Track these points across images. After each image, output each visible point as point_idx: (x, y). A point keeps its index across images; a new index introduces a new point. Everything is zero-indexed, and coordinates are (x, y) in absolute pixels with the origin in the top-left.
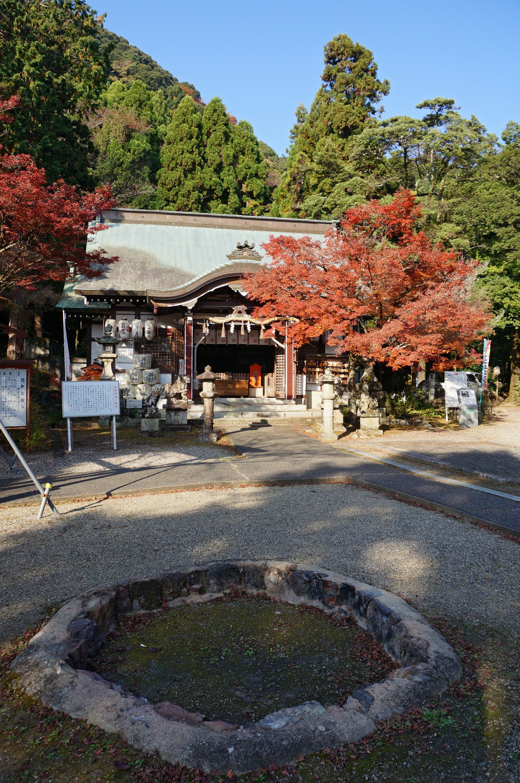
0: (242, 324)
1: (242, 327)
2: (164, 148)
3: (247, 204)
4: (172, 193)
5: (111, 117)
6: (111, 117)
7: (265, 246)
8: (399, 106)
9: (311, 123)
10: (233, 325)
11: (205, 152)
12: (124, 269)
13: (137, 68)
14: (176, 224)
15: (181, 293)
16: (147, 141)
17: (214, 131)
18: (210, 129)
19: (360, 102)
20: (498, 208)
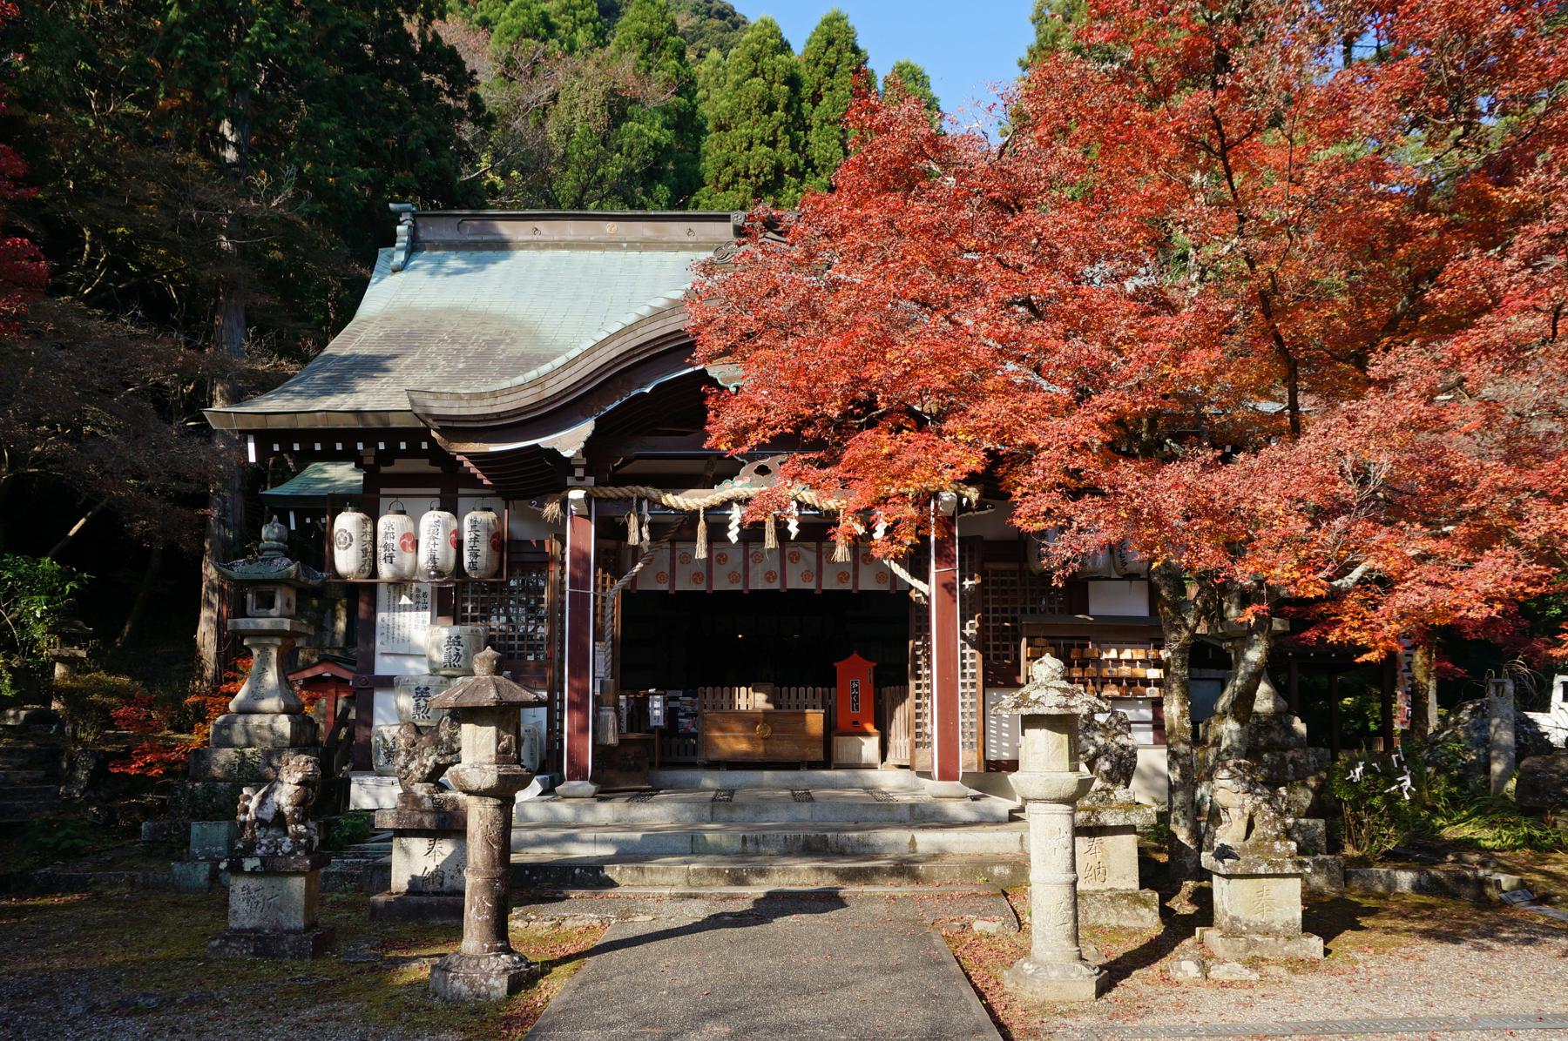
2: (710, 143)
6: (578, 74)
10: (736, 514)
11: (807, 143)
13: (700, 28)
14: (632, 246)
15: (527, 398)
17: (831, 89)
18: (820, 85)
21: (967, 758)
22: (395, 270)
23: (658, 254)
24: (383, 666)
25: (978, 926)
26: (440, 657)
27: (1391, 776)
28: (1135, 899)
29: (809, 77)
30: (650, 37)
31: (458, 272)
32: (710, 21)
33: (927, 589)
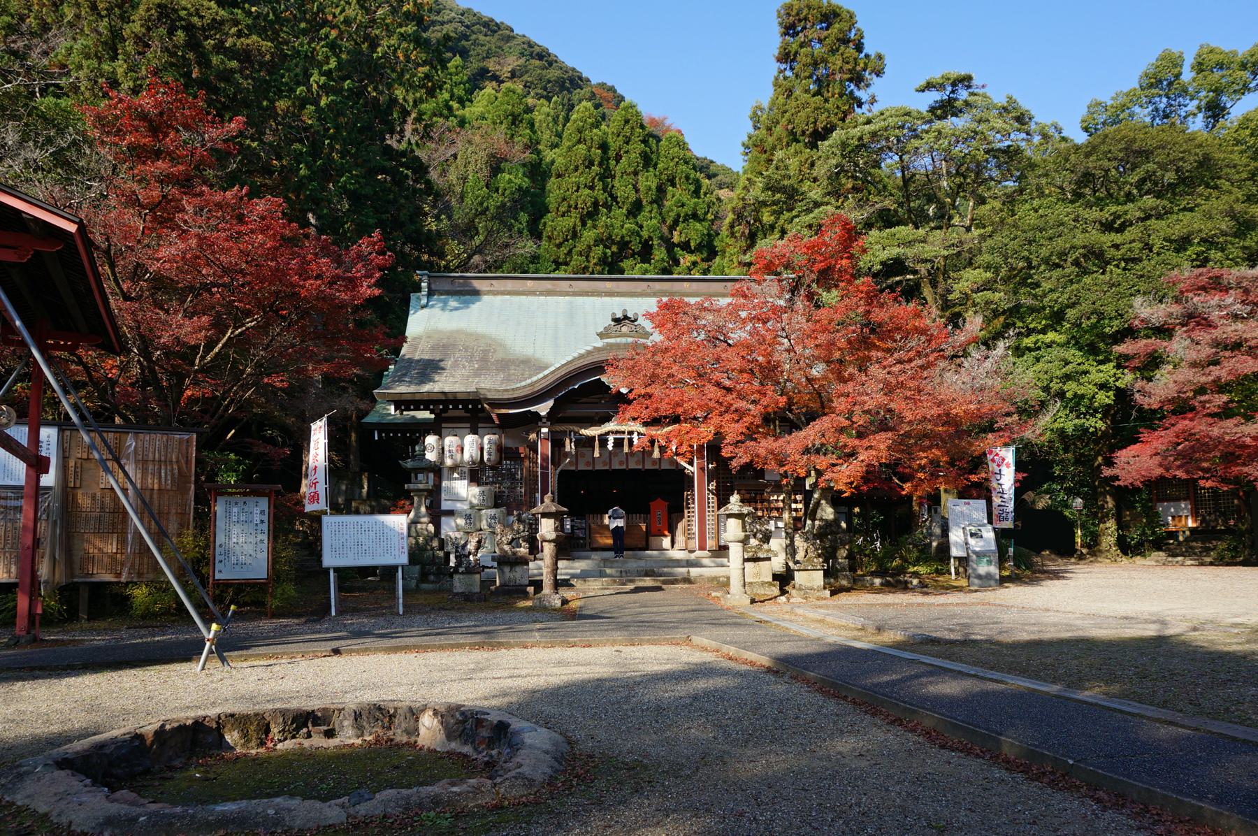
0: (626, 436)
1: (626, 442)
2: (552, 183)
3: (682, 261)
4: (564, 250)
5: (470, 142)
6: (470, 142)
7: (650, 316)
8: (894, 94)
9: (769, 129)
10: (611, 439)
12: (456, 361)
14: (542, 293)
16: (524, 174)
17: (627, 152)
19: (837, 91)
20: (1051, 239)
21: (711, 543)
22: (423, 307)
23: (555, 298)
24: (445, 506)
25: (714, 594)
26: (475, 501)
27: (872, 542)
28: (770, 584)
29: (614, 143)
30: (512, 114)
31: (456, 309)
32: (533, 61)
33: (693, 469)
